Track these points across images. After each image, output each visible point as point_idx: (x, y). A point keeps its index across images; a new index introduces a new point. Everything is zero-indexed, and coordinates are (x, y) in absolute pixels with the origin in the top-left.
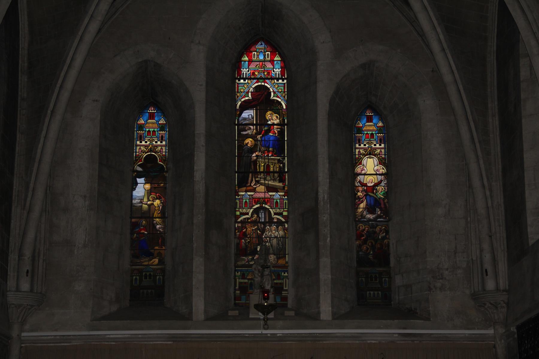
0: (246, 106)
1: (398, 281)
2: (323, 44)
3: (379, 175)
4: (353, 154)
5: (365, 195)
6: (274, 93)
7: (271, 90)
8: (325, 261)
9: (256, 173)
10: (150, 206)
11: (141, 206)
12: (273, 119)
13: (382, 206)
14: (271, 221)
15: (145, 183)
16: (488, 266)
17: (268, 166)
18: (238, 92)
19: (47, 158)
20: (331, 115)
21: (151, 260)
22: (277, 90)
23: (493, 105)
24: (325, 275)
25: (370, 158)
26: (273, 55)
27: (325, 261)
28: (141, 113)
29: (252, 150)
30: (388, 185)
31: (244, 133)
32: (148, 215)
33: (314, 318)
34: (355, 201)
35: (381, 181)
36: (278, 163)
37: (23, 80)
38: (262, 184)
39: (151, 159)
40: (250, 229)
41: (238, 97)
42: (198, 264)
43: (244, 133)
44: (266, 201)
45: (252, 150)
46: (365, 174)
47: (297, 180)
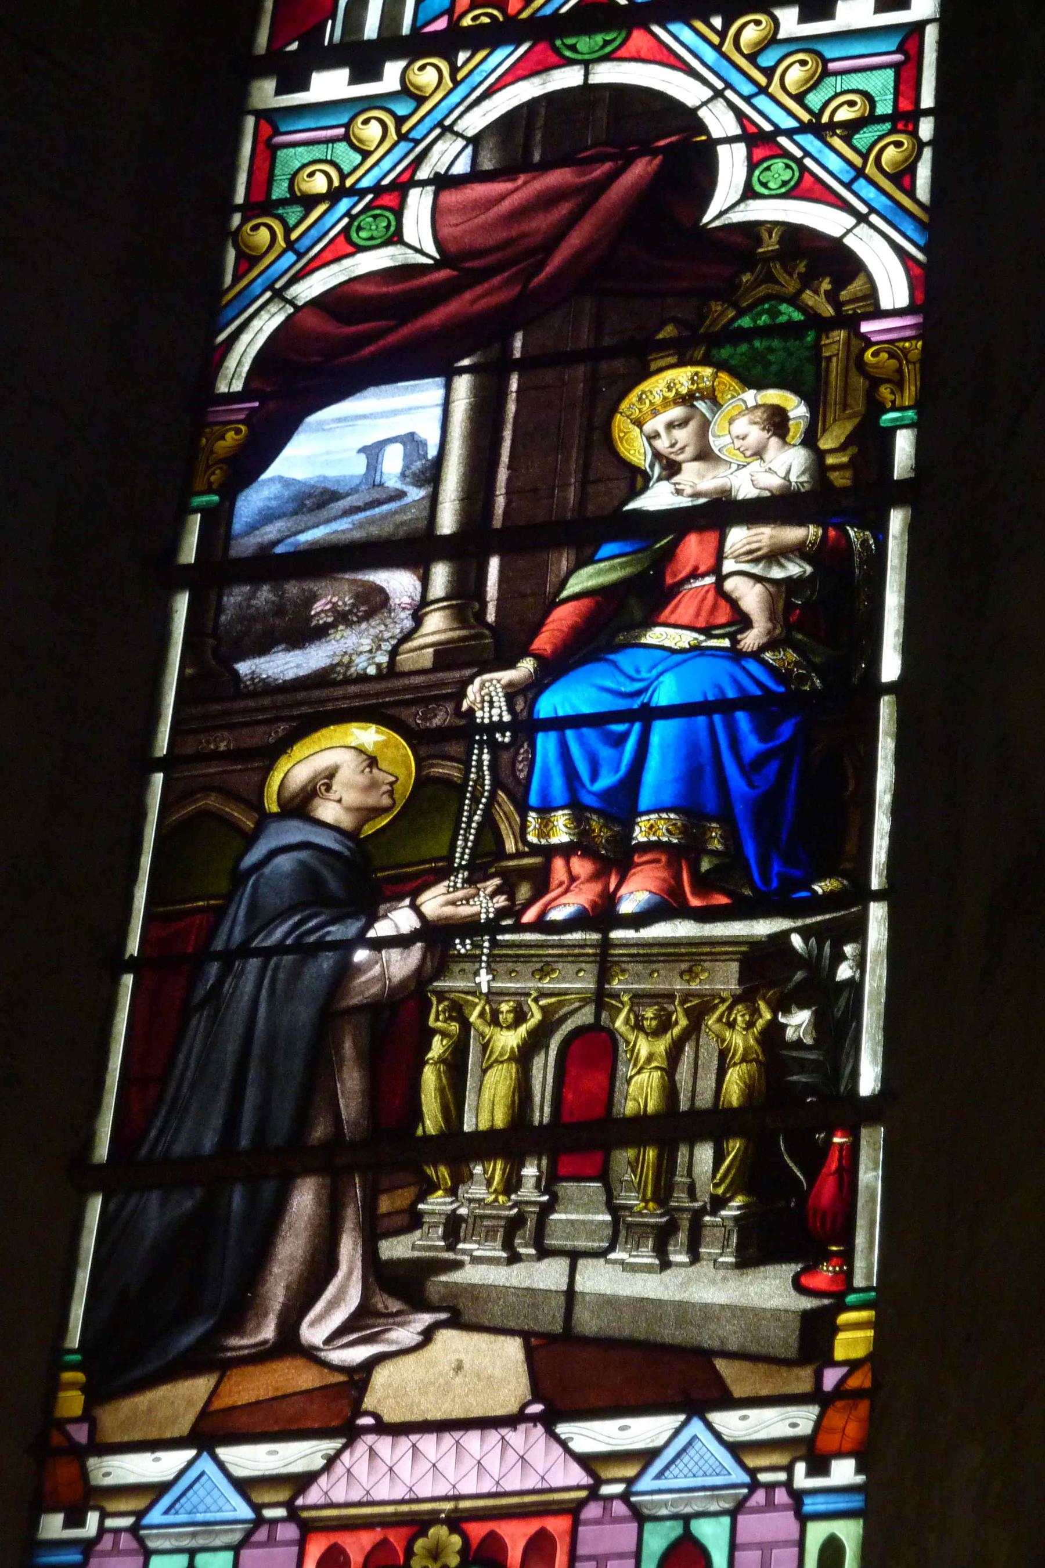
6: (759, 142)
7: (719, 122)
9: (393, 1158)
17: (593, 1052)
18: (261, 205)
29: (365, 871)
31: (284, 665)
36: (746, 997)
38: (462, 1314)
41: (248, 260)
43: (284, 665)
45: (365, 871)
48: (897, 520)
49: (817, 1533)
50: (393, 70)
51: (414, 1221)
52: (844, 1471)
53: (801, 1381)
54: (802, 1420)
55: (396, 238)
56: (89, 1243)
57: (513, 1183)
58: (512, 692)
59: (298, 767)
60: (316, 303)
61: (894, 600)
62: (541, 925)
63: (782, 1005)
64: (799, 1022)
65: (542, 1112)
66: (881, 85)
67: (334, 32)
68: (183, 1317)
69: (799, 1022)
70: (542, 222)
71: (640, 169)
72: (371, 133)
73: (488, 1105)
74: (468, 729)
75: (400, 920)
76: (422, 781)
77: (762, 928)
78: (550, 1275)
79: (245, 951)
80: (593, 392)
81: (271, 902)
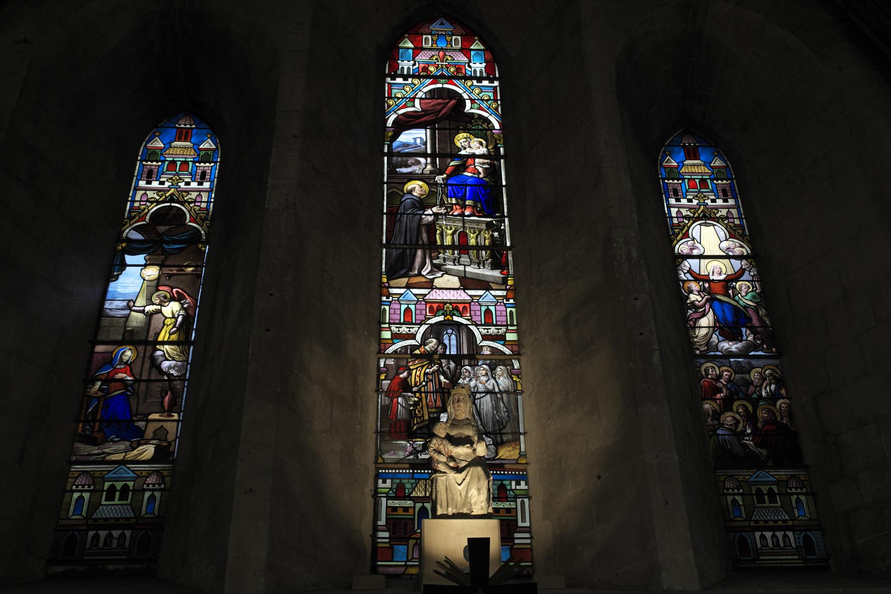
3: (736, 257)
5: (707, 300)
6: (473, 101)
7: (465, 96)
9: (433, 248)
10: (150, 315)
11: (127, 317)
12: (471, 145)
13: (755, 322)
14: (474, 355)
15: (145, 266)
17: (463, 236)
18: (390, 98)
21: (133, 449)
25: (707, 225)
31: (404, 170)
32: (144, 339)
34: (681, 314)
35: (742, 271)
36: (487, 229)
38: (447, 272)
41: (389, 106)
43: (404, 170)
44: (457, 308)
45: (422, 204)
46: (701, 257)
48: (502, 161)
49: (509, 310)
50: (410, 80)
51: (438, 258)
52: (511, 301)
53: (503, 287)
54: (504, 293)
55: (414, 106)
56: (384, 256)
57: (453, 254)
58: (443, 179)
59: (409, 186)
60: (402, 114)
61: (503, 173)
62: (452, 215)
63: (493, 231)
64: (496, 234)
65: (457, 243)
66: (491, 94)
67: (399, 72)
68: (402, 268)
69: (496, 234)
70: (438, 107)
71: (453, 102)
72: (408, 89)
73: (448, 241)
74: (436, 184)
75: (429, 212)
76: (430, 191)
77: (489, 220)
78: (461, 268)
79: (404, 213)
80: (450, 136)
81: (407, 207)
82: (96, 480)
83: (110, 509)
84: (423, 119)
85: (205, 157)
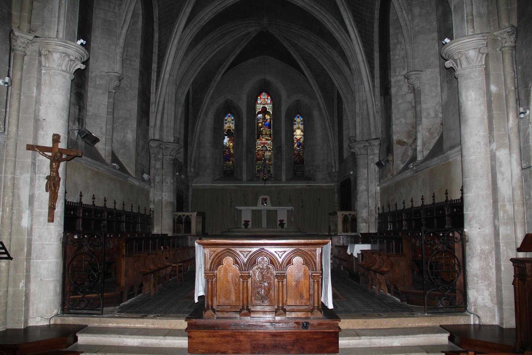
0: (259, 113)
1: (306, 169)
2: (284, 94)
4: (293, 128)
8: (284, 163)
9: (262, 135)
12: (268, 117)
14: (267, 150)
16: (333, 165)
19: (198, 131)
20: (286, 117)
22: (269, 108)
23: (336, 114)
24: (284, 167)
26: (268, 97)
27: (284, 163)
28: (226, 115)
29: (261, 127)
30: (304, 138)
32: (228, 148)
33: (280, 181)
34: (293, 143)
37: (191, 106)
39: (229, 130)
40: (260, 152)
42: (244, 164)
44: (265, 143)
47: (276, 138)
82: (226, 166)
83: (228, 169)
84: (303, 241)
85: (233, 120)
